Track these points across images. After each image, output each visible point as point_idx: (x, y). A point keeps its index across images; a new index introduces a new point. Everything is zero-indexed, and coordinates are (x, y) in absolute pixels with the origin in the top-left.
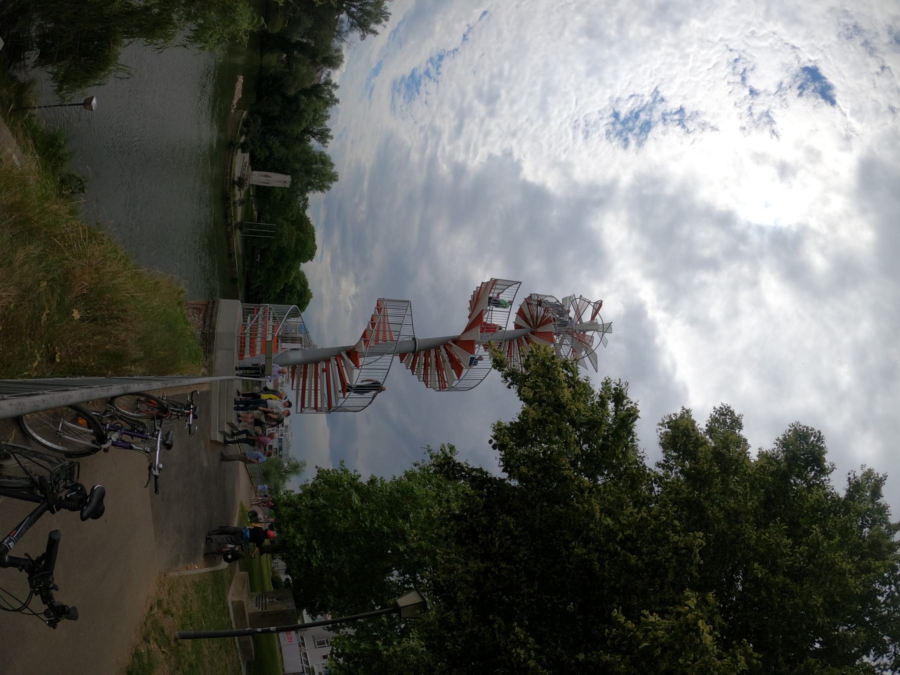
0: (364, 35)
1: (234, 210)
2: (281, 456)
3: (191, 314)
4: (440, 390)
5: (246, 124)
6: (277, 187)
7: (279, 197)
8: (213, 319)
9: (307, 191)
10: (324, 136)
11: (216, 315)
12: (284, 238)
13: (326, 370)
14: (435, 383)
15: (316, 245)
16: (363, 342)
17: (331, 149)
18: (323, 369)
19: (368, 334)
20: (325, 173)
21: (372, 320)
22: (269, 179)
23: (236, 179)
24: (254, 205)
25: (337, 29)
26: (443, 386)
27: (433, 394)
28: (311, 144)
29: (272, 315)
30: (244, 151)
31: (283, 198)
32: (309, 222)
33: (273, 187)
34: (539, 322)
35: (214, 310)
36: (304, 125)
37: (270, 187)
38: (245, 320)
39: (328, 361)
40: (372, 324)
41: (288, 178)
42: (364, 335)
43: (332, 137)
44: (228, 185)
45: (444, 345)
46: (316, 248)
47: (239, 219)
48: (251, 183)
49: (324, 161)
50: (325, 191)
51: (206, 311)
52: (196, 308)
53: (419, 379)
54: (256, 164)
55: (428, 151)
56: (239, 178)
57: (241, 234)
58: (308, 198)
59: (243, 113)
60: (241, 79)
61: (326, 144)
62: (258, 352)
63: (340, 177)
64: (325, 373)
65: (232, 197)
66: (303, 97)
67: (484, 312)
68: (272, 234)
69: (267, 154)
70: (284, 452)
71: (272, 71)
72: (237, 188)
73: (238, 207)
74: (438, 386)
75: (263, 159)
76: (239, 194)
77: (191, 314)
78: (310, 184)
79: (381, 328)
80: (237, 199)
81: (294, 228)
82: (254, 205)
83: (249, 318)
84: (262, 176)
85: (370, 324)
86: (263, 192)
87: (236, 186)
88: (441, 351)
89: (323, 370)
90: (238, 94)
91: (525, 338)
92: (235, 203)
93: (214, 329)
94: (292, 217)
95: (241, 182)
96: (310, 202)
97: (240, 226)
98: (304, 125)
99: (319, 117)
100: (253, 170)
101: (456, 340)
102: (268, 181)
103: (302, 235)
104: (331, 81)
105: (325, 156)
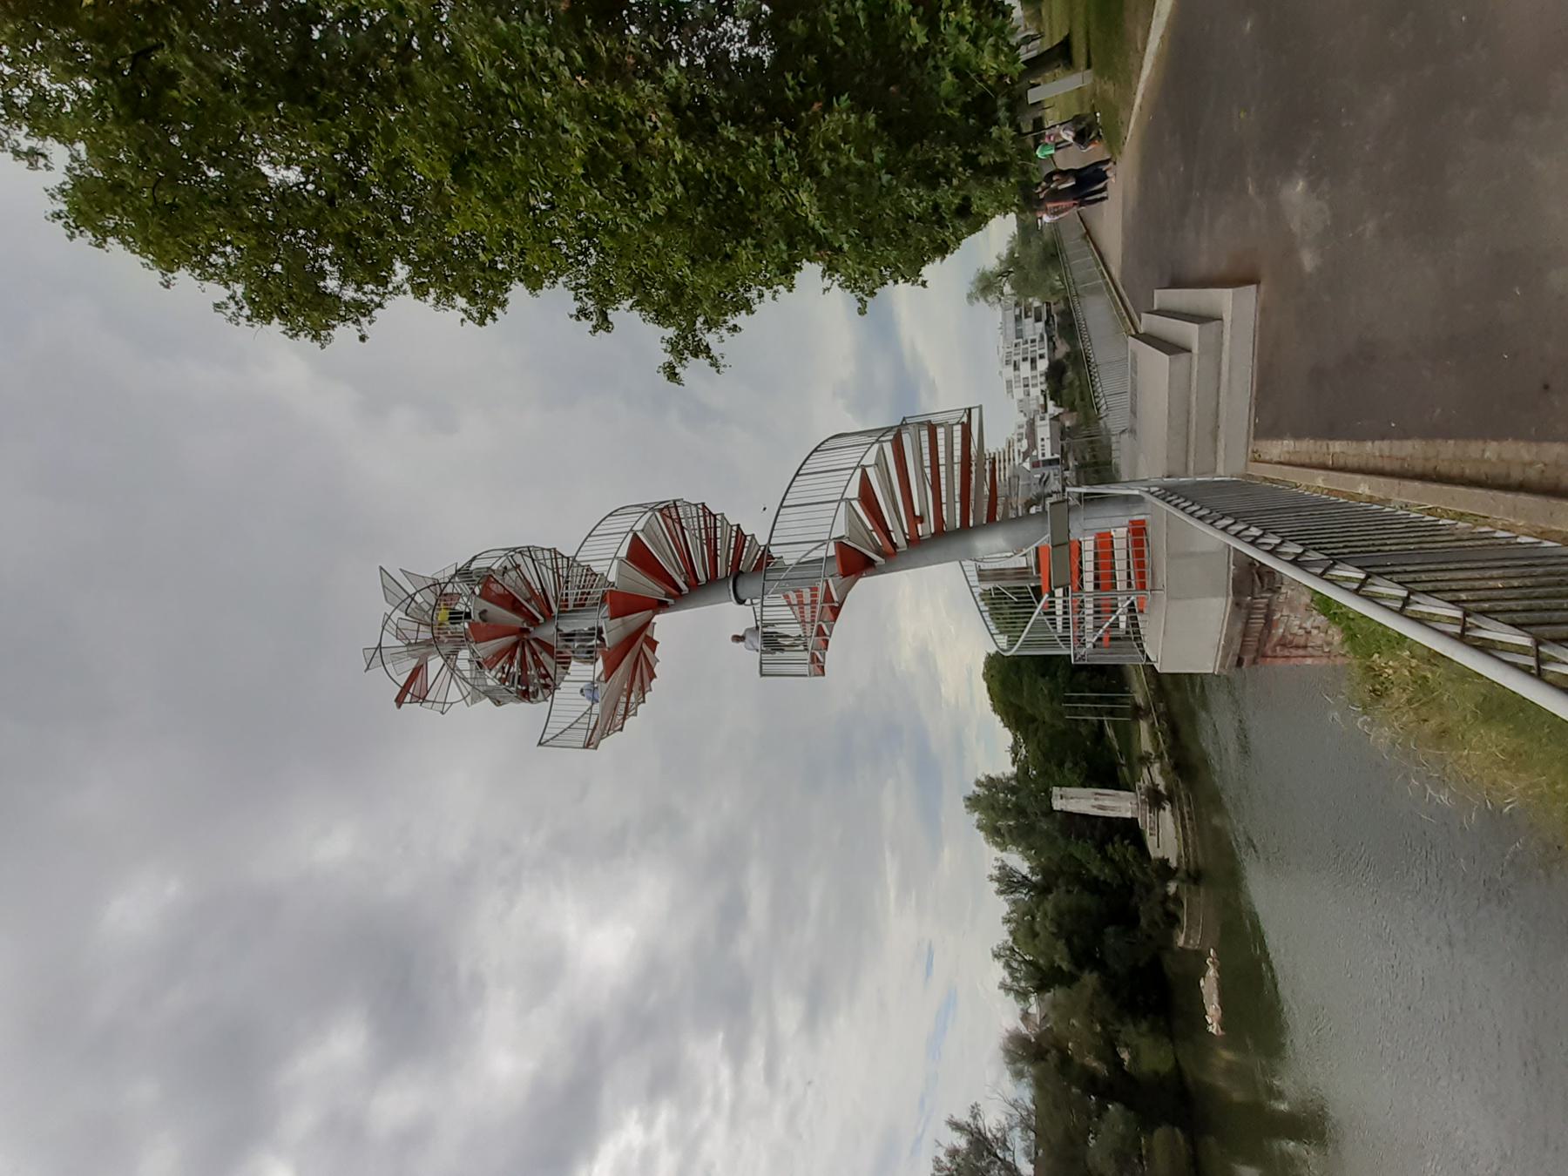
0: (974, 1118)
1: (1158, 744)
2: (1017, 304)
3: (1315, 632)
4: (675, 502)
5: (1173, 920)
6: (1075, 786)
7: (1068, 765)
8: (1239, 626)
9: (1016, 775)
10: (1008, 882)
11: (1229, 641)
12: (1046, 692)
13: (916, 519)
14: (685, 514)
15: (985, 679)
16: (836, 598)
17: (990, 857)
18: (922, 522)
19: (828, 615)
20: (990, 812)
21: (827, 642)
22: (1097, 803)
23: (1168, 807)
24: (1117, 747)
25: (1032, 1135)
26: (668, 511)
27: (689, 491)
28: (1027, 864)
29: (1059, 621)
30: (1164, 862)
31: (1061, 765)
32: (1003, 720)
33: (1084, 786)
34: (518, 650)
35: (1236, 647)
36: (1048, 905)
37: (1090, 786)
38: (1134, 623)
39: (914, 541)
40: (825, 635)
41: (1058, 805)
42: (836, 612)
43: (991, 878)
44: (1182, 794)
45: (681, 595)
46: (984, 674)
47: (1144, 726)
48: (1132, 794)
49: (995, 833)
50: (983, 779)
51: (1262, 641)
52: (1297, 647)
53: (723, 517)
54: (1129, 830)
55: (757, 1060)
56: (1161, 808)
57: (1133, 698)
58: (1013, 764)
59: (1186, 942)
60: (1214, 1028)
61: (999, 864)
62: (1089, 546)
63: (962, 804)
64: (917, 513)
65: (1169, 769)
66: (1065, 966)
67: (603, 678)
68: (1069, 700)
69: (1109, 848)
70: (1011, 314)
71: (1144, 1026)
72: (1162, 788)
73: (1151, 751)
74: (680, 510)
75: (1116, 838)
76: (1155, 775)
77: (1315, 632)
78: (1013, 790)
79: (808, 610)
80: (1156, 767)
81: (1030, 711)
82: (1117, 747)
83: (1123, 625)
84: (1113, 809)
85: (827, 632)
86: (1105, 775)
87: (1163, 791)
88: (685, 583)
89: (921, 519)
90: (1209, 985)
91: (538, 620)
92: (1160, 757)
93: (1237, 604)
94: (1037, 730)
95: (1155, 799)
96: (1009, 758)
97: (1137, 714)
98: (1048, 905)
99: (1024, 928)
100: (1134, 820)
101: (661, 606)
102: (1096, 799)
103: (1012, 699)
104: (1015, 997)
105: (996, 844)
